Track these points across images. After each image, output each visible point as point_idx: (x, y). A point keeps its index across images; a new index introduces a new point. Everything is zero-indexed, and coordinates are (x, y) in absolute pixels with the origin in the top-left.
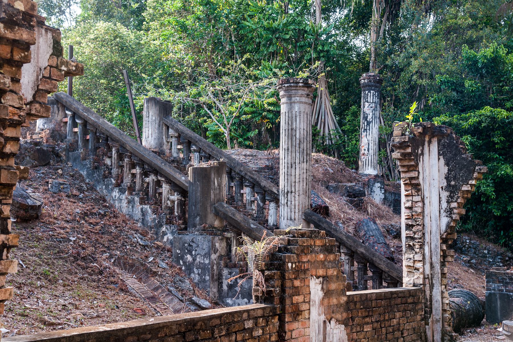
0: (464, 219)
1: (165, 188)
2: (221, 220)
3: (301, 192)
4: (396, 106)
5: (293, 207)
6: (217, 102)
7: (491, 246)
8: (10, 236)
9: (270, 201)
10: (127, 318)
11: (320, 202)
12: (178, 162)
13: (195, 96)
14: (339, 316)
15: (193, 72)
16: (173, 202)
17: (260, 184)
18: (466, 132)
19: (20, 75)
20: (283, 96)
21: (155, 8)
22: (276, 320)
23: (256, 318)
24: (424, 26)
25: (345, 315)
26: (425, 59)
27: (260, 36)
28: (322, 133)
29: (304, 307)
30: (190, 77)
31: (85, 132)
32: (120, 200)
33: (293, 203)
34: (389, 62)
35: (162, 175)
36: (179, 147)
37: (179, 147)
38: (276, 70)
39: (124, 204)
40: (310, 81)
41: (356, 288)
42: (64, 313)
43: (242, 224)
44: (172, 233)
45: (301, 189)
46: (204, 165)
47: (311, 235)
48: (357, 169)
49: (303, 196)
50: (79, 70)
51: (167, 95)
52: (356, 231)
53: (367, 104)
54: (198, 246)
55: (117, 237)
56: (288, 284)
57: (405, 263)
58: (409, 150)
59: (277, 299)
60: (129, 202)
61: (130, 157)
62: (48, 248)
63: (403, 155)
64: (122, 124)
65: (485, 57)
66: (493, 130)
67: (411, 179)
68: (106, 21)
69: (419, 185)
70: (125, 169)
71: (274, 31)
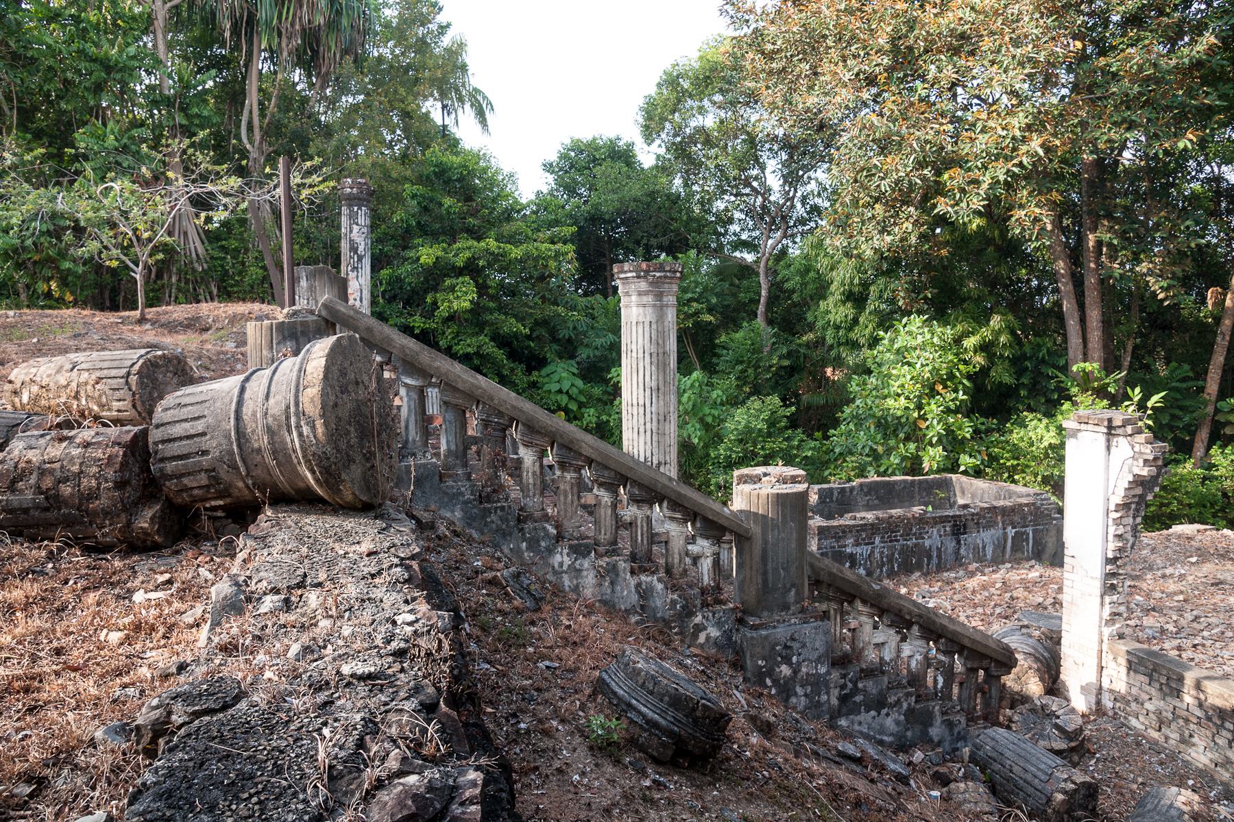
32: (576, 572)
44: (719, 624)
54: (804, 646)
60: (600, 576)
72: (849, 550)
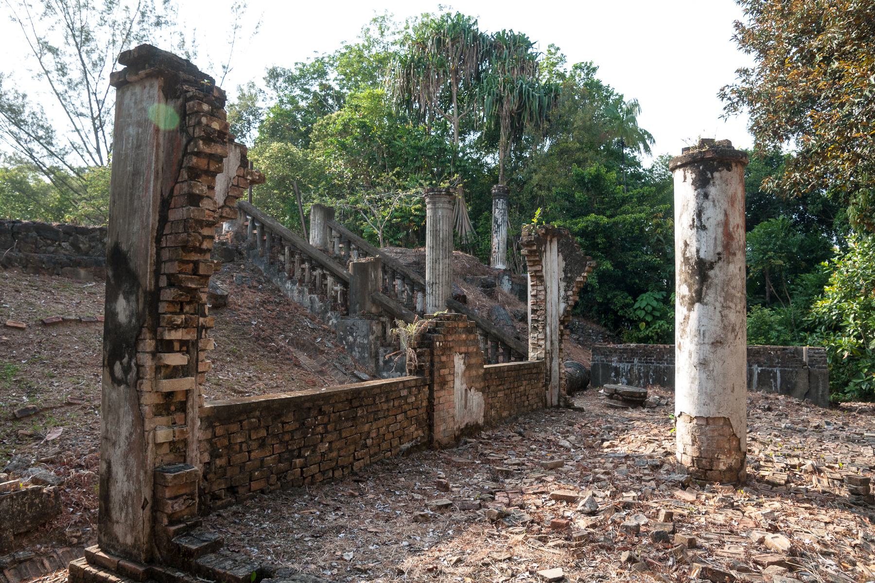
0: (576, 305)
1: (330, 280)
2: (377, 307)
4: (520, 213)
6: (372, 208)
7: (595, 326)
8: (207, 319)
9: (418, 291)
10: (301, 388)
11: (459, 292)
12: (340, 258)
13: (352, 204)
14: (477, 385)
15: (351, 183)
16: (336, 292)
18: (576, 234)
19: (215, 183)
20: (429, 203)
21: (320, 130)
22: (426, 389)
23: (410, 388)
24: (543, 147)
25: (482, 384)
26: (544, 174)
27: (407, 153)
29: (449, 378)
30: (349, 187)
31: (262, 233)
32: (292, 290)
34: (514, 176)
35: (327, 270)
36: (341, 246)
37: (341, 246)
38: (422, 181)
39: (296, 294)
40: (451, 190)
41: (490, 363)
42: (249, 384)
43: (395, 310)
44: (336, 318)
46: (363, 260)
47: (455, 319)
48: (489, 264)
50: (262, 179)
51: (330, 202)
52: (489, 316)
53: (497, 210)
55: (290, 321)
56: (436, 359)
57: (530, 341)
58: (535, 248)
59: (427, 372)
60: (300, 292)
61: (300, 254)
62: (234, 330)
63: (530, 252)
64: (292, 227)
65: (590, 174)
66: (597, 233)
67: (536, 271)
68: (278, 141)
69: (542, 276)
70: (296, 264)
71: (419, 149)
72: (614, 364)
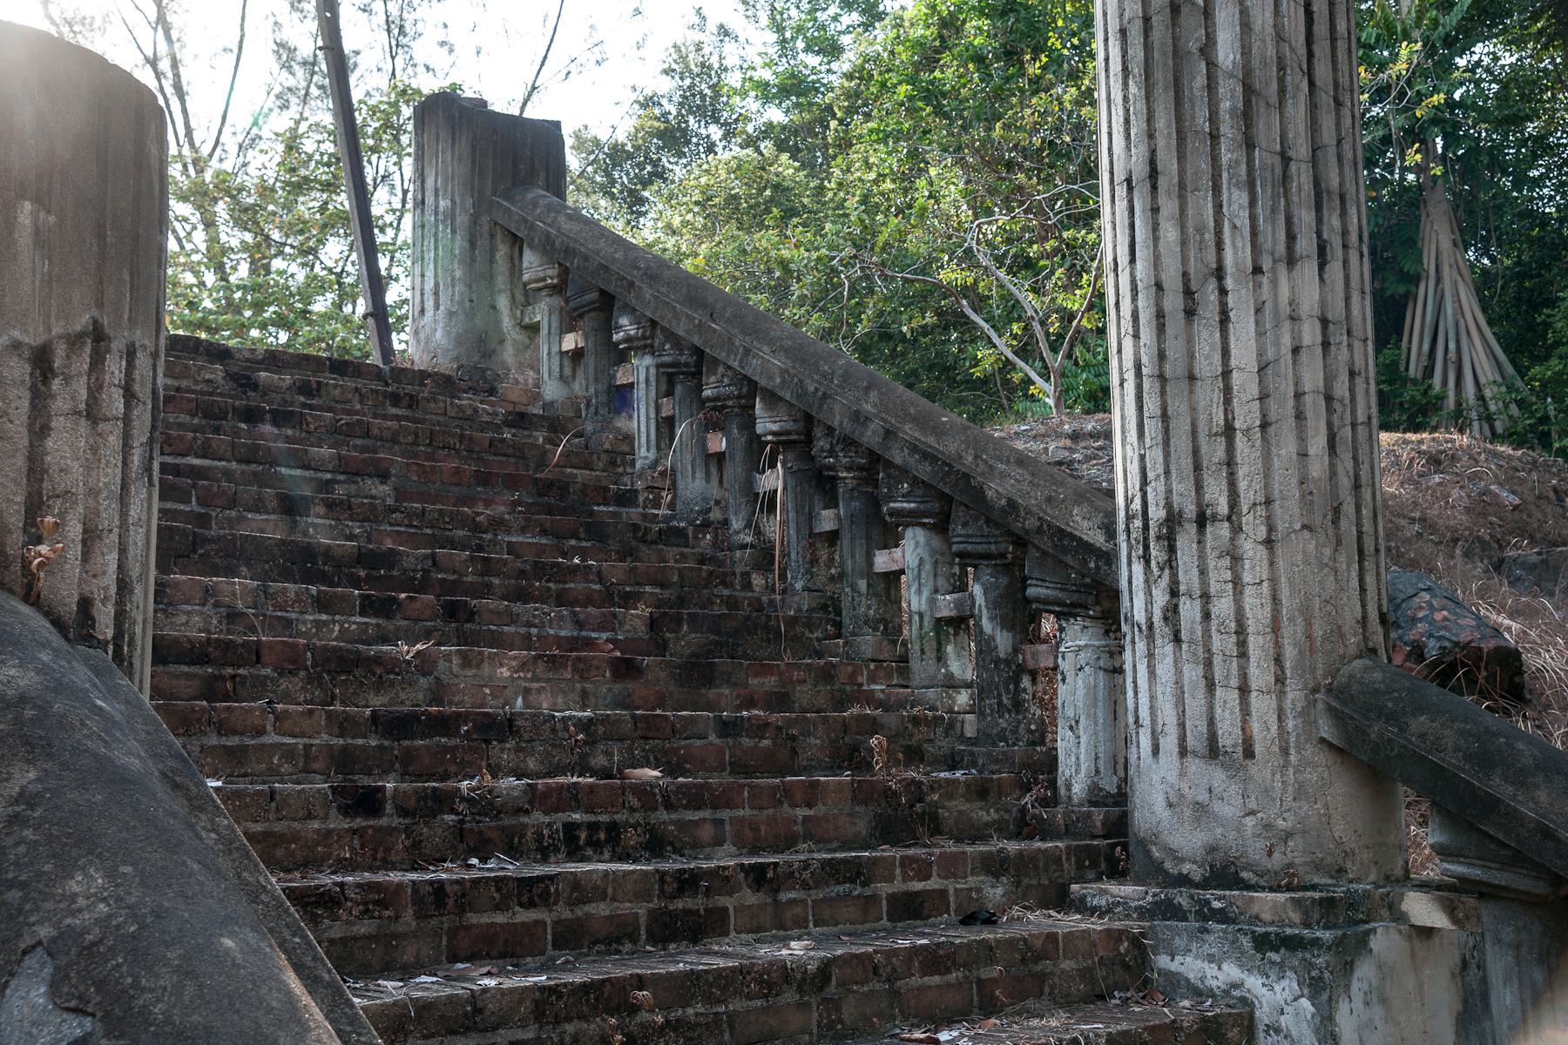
3: (1288, 515)
5: (1222, 644)
9: (1066, 613)
11: (1466, 631)
17: (978, 495)
28: (1451, 402)
33: (1223, 607)
45: (1285, 481)
49: (1307, 544)
